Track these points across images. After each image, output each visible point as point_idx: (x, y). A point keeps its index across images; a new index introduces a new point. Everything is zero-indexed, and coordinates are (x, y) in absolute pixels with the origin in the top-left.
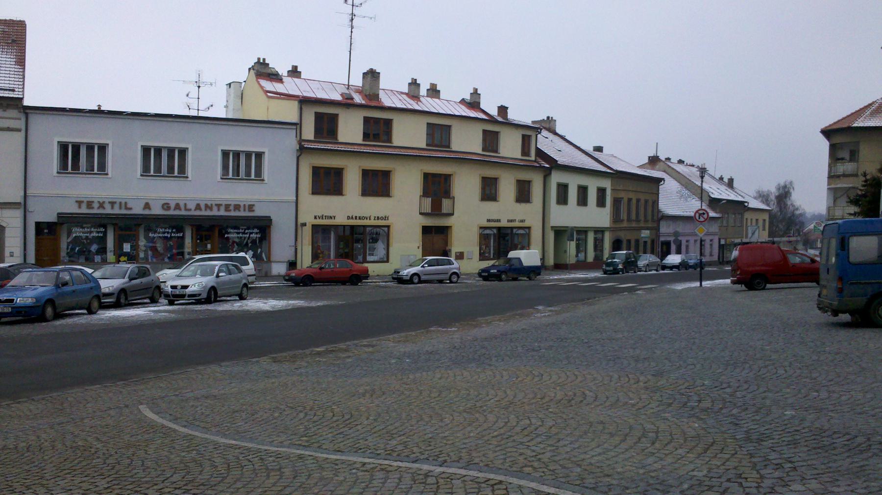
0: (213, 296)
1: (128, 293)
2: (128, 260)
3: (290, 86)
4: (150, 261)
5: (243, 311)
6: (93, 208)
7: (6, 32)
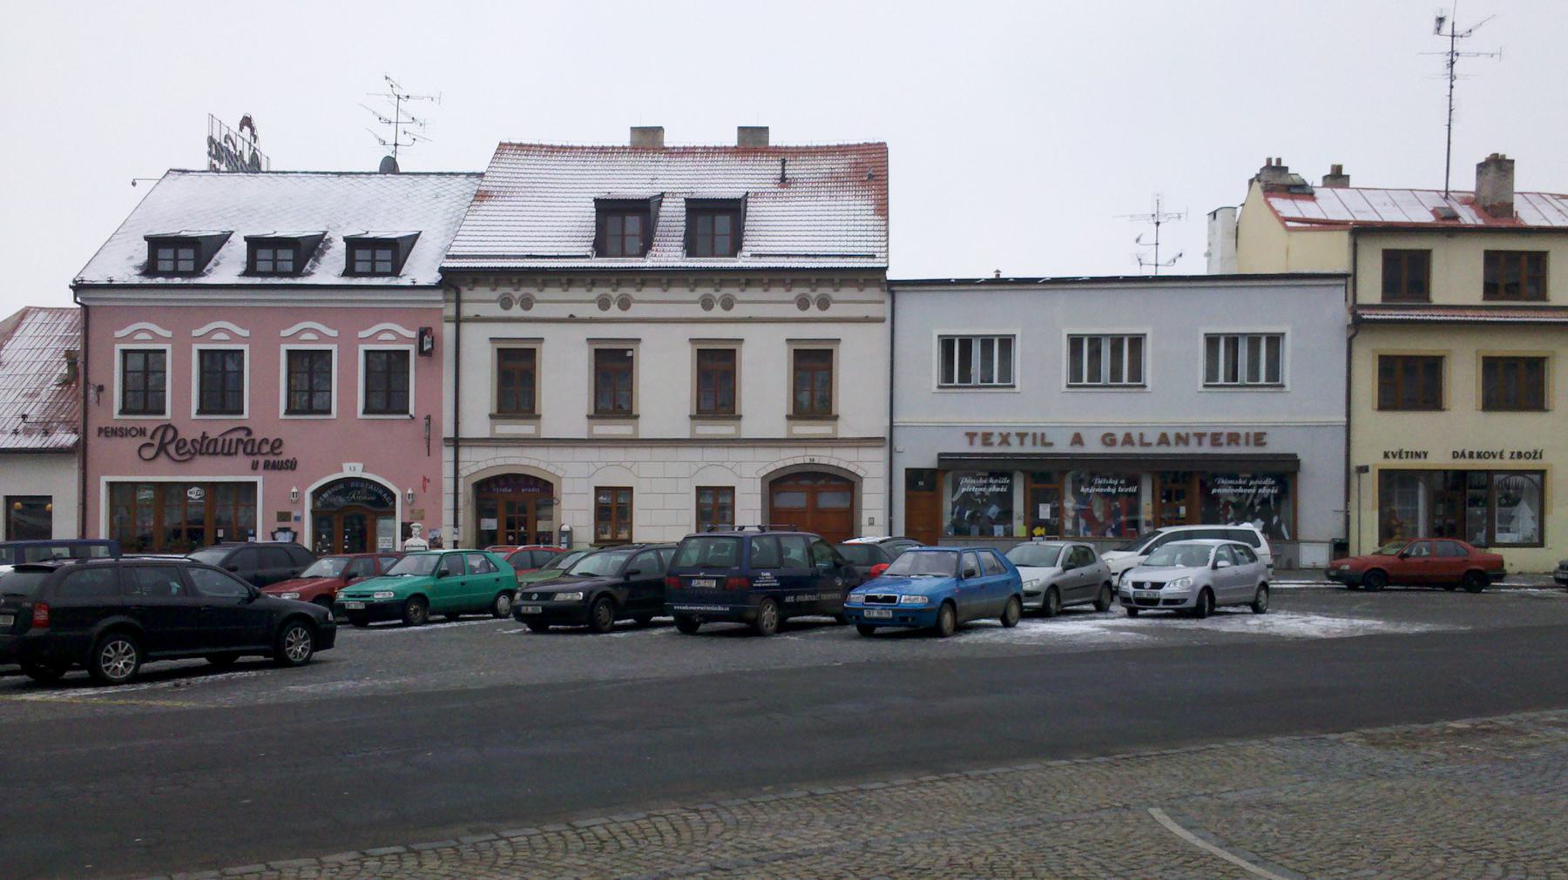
0: (1207, 604)
1: (1061, 590)
2: (1047, 533)
3: (1329, 205)
4: (1082, 535)
5: (1269, 635)
6: (991, 444)
7: (860, 163)
